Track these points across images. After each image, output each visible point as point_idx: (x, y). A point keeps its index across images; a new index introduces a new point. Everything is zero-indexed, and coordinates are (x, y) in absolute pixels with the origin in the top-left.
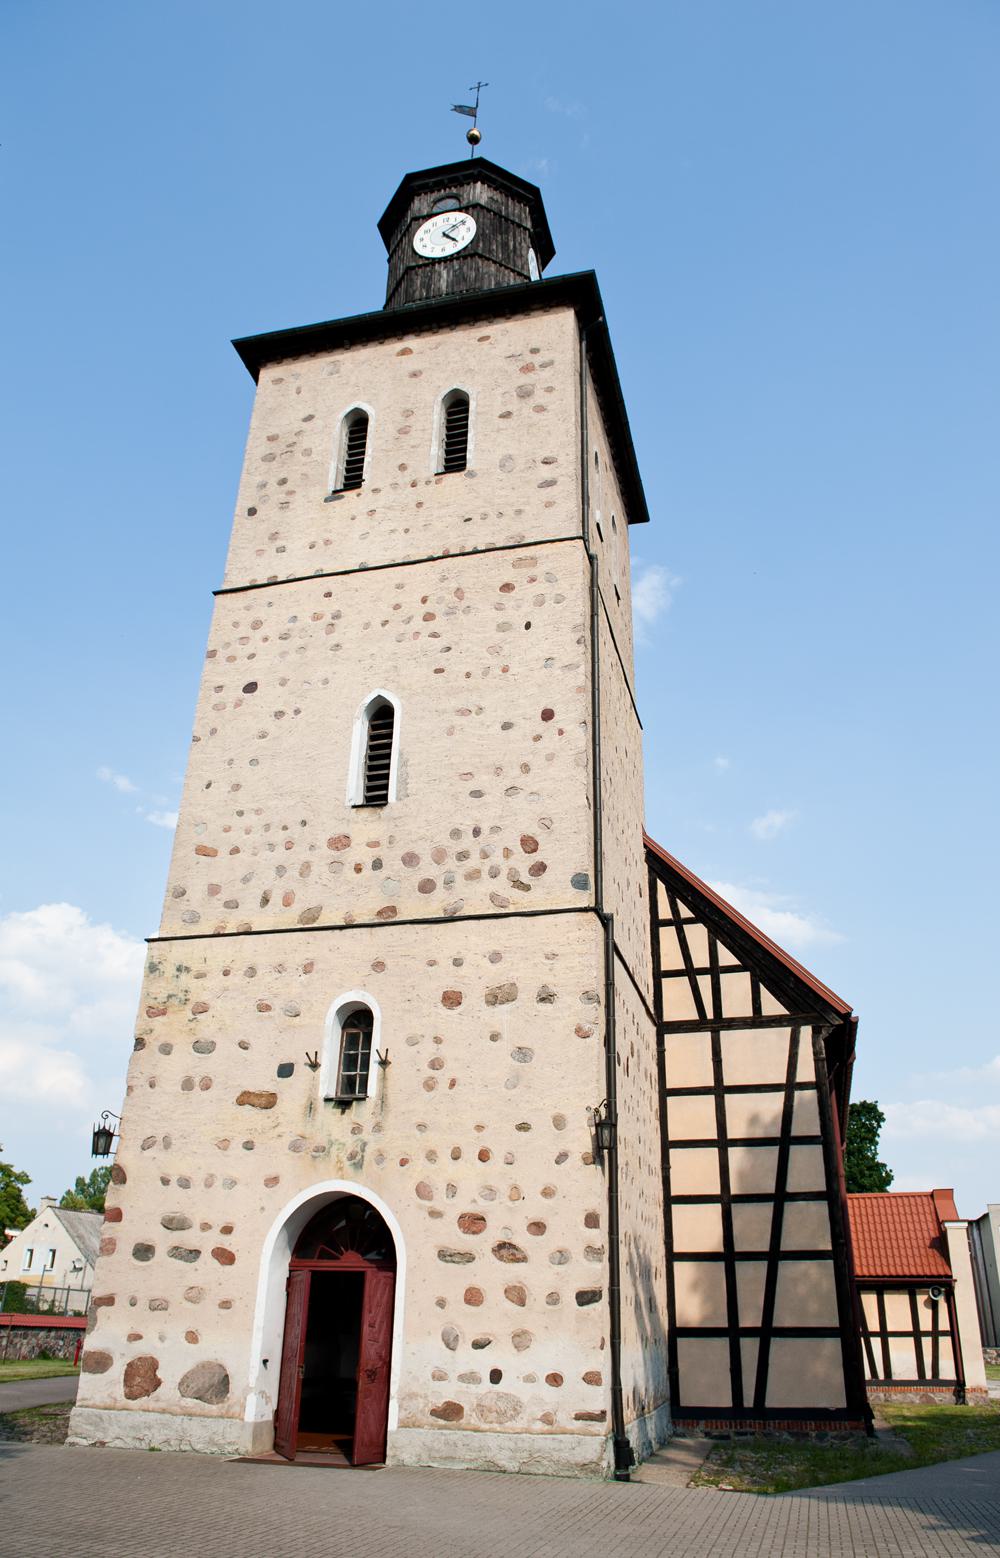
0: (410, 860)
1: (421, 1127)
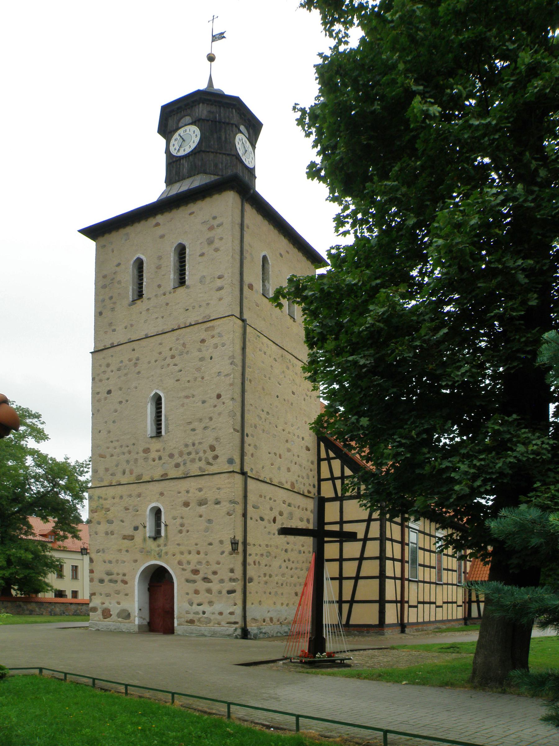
0: (171, 456)
1: (178, 545)
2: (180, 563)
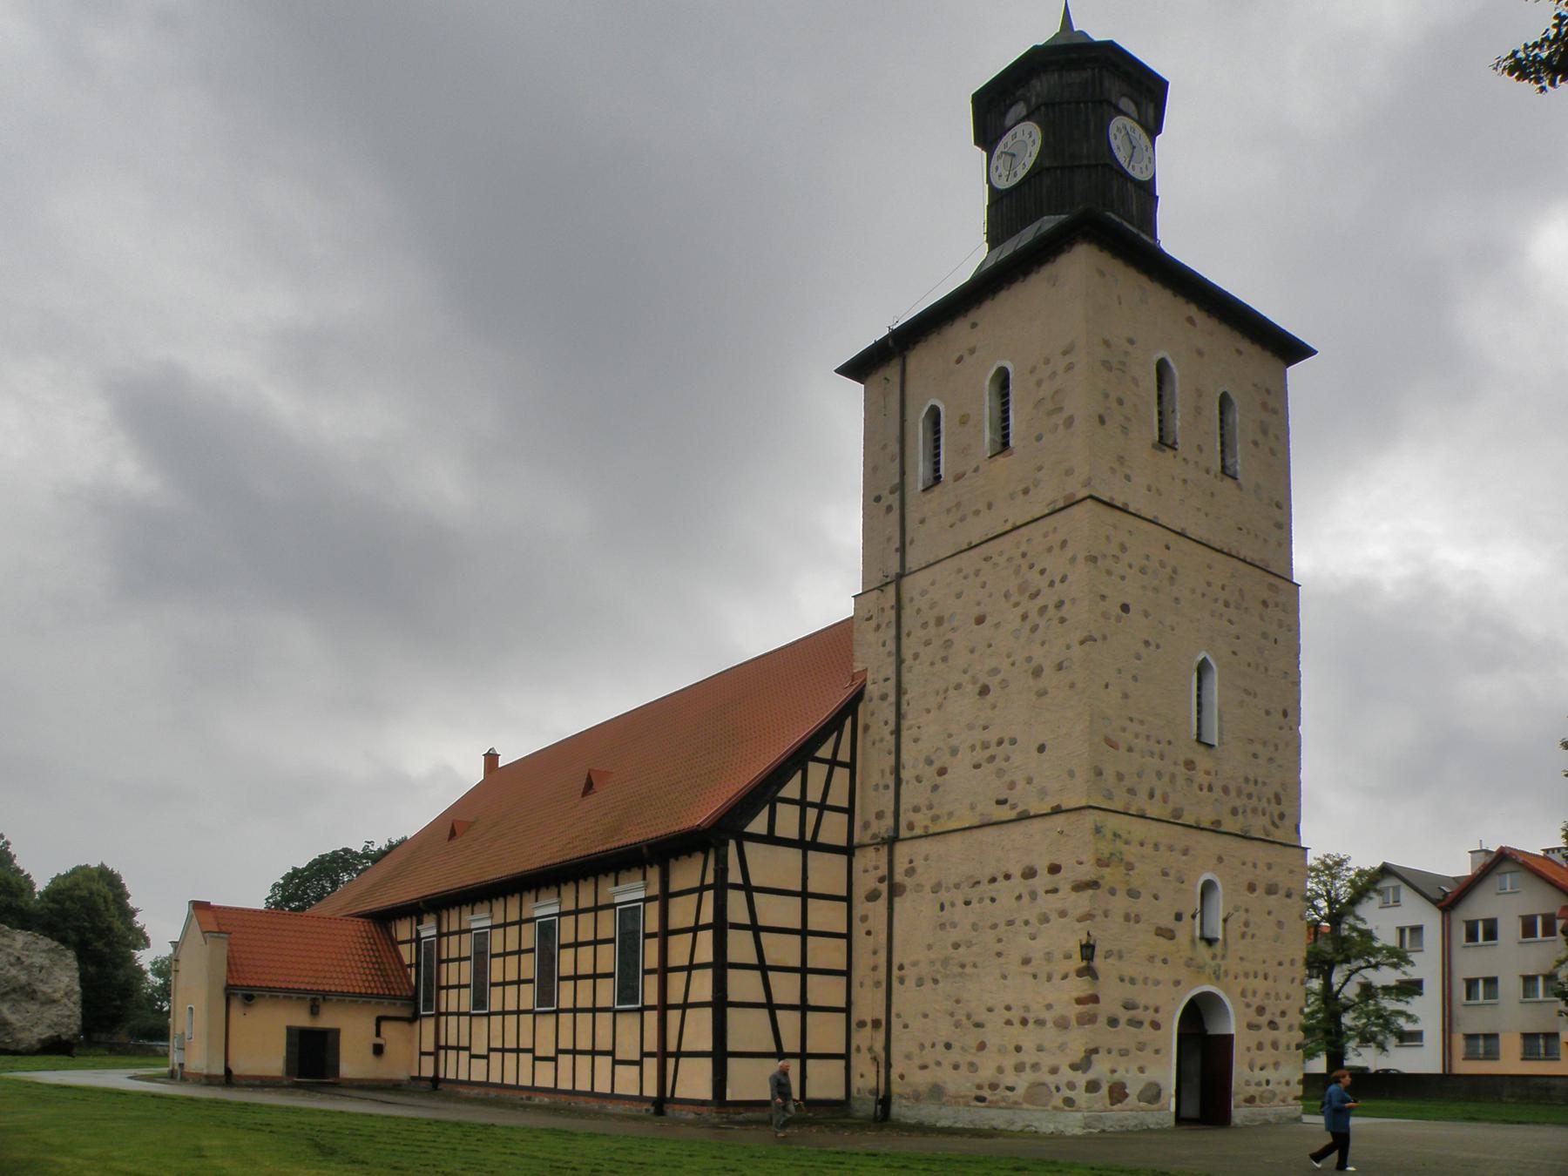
0: (1226, 790)
2: (1243, 994)
